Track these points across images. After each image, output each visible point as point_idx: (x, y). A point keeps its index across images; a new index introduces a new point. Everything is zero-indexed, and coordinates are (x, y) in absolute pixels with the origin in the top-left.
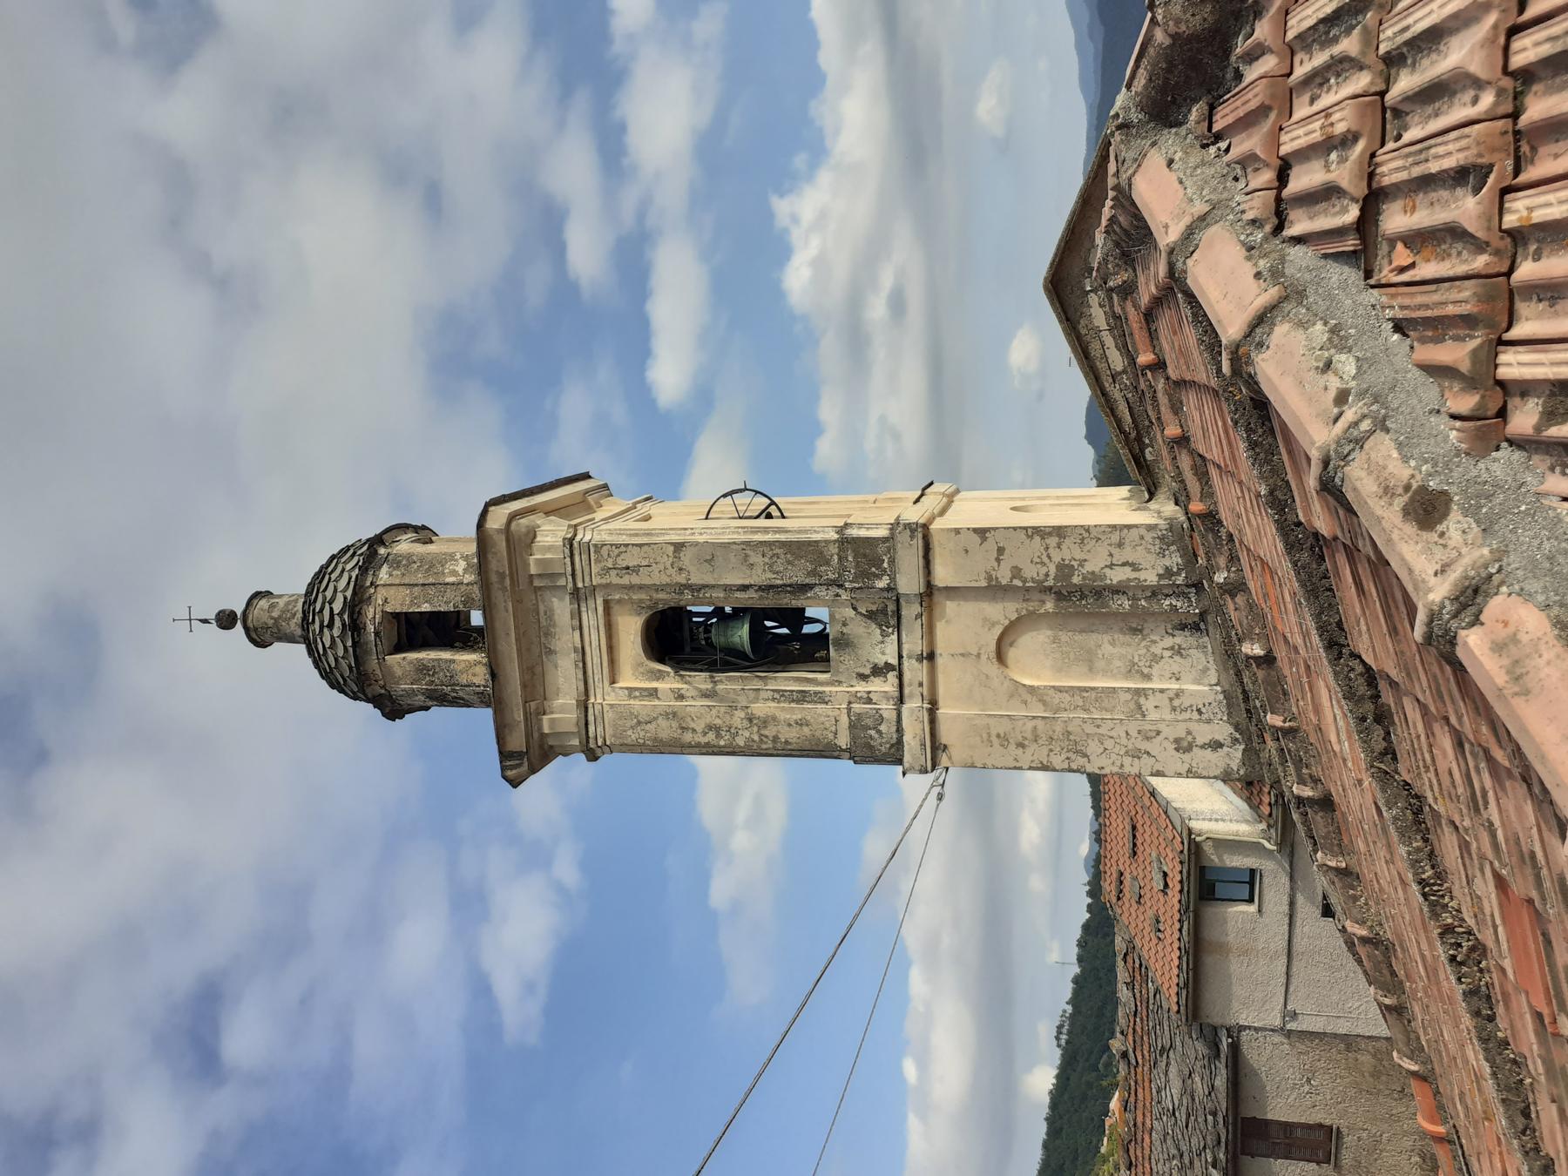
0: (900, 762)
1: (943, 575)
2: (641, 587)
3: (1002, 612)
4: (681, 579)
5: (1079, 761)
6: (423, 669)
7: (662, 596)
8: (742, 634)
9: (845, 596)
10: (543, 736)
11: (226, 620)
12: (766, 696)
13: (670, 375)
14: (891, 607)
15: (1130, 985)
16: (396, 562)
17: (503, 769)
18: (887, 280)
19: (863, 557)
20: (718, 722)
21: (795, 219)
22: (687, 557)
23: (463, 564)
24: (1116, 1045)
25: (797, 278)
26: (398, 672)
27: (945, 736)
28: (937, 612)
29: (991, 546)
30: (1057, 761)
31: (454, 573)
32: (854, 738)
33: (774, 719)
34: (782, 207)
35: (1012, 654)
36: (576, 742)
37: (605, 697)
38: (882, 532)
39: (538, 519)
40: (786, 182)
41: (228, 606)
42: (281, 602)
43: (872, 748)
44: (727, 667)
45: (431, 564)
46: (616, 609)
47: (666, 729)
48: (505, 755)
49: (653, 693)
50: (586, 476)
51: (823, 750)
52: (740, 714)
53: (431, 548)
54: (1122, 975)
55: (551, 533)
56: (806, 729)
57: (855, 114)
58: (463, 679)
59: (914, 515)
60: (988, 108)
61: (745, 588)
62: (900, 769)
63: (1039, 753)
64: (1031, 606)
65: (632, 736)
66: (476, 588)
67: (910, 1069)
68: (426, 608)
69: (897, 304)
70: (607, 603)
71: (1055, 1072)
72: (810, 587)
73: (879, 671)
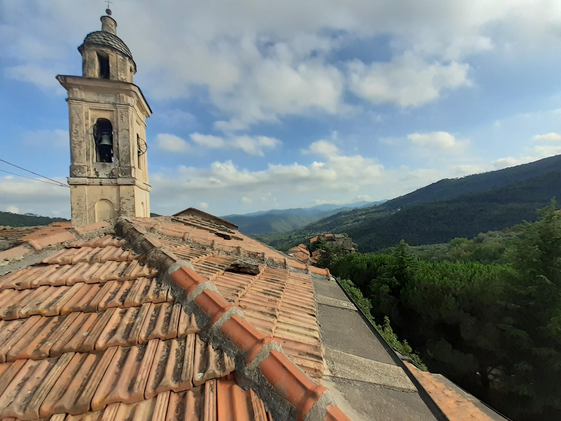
0: (71, 177)
1: (122, 188)
2: (117, 120)
3: (114, 200)
4: (120, 130)
5: (74, 216)
6: (93, 61)
7: (115, 124)
8: (106, 142)
9: (117, 167)
10: (72, 88)
11: (108, 11)
12: (88, 145)
13: (197, 137)
14: (114, 177)
15: (27, 230)
16: (124, 61)
17: (61, 76)
18: (218, 181)
19: (127, 172)
20: (79, 134)
21: (228, 164)
22: (126, 132)
23: (124, 78)
24: (8, 227)
25: (217, 165)
26: (91, 54)
27: (78, 187)
28: (114, 187)
29: (130, 198)
30: (74, 212)
31: (121, 75)
32: (76, 166)
33: (81, 148)
34: (230, 162)
35: (104, 202)
36: (71, 96)
37: (85, 107)
38: (133, 175)
39: (136, 98)
40: (235, 162)
41: (112, 13)
42: (113, 28)
43: (73, 171)
44: (96, 138)
45: (124, 70)
46: (111, 113)
47: (76, 120)
48: (65, 76)
49: (87, 118)
50: (151, 112)
51: (73, 159)
52: (82, 139)
53: (129, 71)
54: (30, 228)
55: (132, 101)
56: (78, 155)
57: (246, 177)
58: (90, 70)
59: (137, 182)
60: (245, 199)
61: (118, 144)
62: (69, 176)
63: (76, 207)
64: (116, 206)
65: (74, 112)
66: (116, 80)
67: (9, 177)
68: (111, 65)
69: (213, 183)
70: (113, 111)
71: (17, 213)
72: (119, 159)
73: (97, 173)
